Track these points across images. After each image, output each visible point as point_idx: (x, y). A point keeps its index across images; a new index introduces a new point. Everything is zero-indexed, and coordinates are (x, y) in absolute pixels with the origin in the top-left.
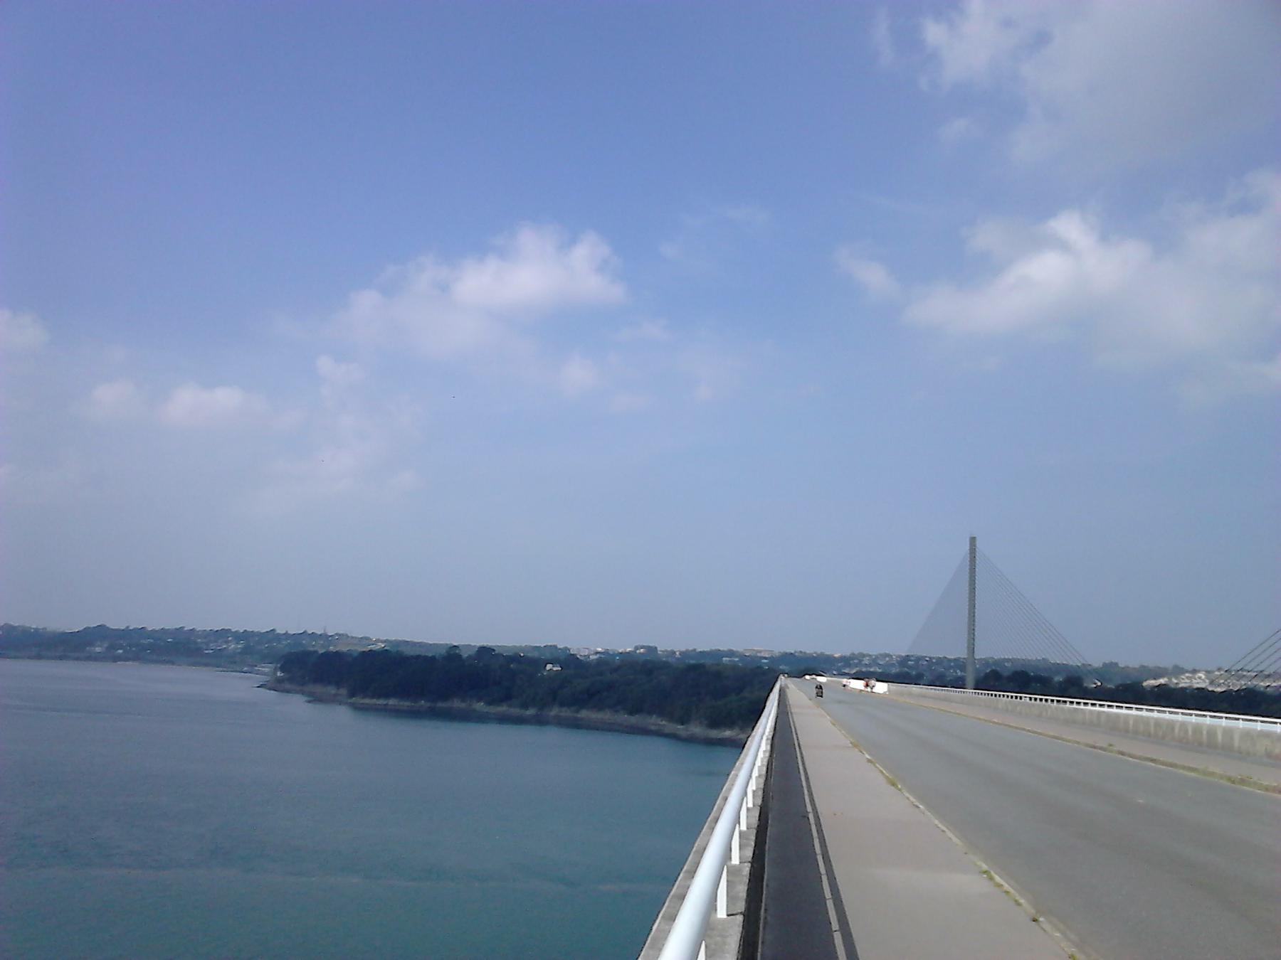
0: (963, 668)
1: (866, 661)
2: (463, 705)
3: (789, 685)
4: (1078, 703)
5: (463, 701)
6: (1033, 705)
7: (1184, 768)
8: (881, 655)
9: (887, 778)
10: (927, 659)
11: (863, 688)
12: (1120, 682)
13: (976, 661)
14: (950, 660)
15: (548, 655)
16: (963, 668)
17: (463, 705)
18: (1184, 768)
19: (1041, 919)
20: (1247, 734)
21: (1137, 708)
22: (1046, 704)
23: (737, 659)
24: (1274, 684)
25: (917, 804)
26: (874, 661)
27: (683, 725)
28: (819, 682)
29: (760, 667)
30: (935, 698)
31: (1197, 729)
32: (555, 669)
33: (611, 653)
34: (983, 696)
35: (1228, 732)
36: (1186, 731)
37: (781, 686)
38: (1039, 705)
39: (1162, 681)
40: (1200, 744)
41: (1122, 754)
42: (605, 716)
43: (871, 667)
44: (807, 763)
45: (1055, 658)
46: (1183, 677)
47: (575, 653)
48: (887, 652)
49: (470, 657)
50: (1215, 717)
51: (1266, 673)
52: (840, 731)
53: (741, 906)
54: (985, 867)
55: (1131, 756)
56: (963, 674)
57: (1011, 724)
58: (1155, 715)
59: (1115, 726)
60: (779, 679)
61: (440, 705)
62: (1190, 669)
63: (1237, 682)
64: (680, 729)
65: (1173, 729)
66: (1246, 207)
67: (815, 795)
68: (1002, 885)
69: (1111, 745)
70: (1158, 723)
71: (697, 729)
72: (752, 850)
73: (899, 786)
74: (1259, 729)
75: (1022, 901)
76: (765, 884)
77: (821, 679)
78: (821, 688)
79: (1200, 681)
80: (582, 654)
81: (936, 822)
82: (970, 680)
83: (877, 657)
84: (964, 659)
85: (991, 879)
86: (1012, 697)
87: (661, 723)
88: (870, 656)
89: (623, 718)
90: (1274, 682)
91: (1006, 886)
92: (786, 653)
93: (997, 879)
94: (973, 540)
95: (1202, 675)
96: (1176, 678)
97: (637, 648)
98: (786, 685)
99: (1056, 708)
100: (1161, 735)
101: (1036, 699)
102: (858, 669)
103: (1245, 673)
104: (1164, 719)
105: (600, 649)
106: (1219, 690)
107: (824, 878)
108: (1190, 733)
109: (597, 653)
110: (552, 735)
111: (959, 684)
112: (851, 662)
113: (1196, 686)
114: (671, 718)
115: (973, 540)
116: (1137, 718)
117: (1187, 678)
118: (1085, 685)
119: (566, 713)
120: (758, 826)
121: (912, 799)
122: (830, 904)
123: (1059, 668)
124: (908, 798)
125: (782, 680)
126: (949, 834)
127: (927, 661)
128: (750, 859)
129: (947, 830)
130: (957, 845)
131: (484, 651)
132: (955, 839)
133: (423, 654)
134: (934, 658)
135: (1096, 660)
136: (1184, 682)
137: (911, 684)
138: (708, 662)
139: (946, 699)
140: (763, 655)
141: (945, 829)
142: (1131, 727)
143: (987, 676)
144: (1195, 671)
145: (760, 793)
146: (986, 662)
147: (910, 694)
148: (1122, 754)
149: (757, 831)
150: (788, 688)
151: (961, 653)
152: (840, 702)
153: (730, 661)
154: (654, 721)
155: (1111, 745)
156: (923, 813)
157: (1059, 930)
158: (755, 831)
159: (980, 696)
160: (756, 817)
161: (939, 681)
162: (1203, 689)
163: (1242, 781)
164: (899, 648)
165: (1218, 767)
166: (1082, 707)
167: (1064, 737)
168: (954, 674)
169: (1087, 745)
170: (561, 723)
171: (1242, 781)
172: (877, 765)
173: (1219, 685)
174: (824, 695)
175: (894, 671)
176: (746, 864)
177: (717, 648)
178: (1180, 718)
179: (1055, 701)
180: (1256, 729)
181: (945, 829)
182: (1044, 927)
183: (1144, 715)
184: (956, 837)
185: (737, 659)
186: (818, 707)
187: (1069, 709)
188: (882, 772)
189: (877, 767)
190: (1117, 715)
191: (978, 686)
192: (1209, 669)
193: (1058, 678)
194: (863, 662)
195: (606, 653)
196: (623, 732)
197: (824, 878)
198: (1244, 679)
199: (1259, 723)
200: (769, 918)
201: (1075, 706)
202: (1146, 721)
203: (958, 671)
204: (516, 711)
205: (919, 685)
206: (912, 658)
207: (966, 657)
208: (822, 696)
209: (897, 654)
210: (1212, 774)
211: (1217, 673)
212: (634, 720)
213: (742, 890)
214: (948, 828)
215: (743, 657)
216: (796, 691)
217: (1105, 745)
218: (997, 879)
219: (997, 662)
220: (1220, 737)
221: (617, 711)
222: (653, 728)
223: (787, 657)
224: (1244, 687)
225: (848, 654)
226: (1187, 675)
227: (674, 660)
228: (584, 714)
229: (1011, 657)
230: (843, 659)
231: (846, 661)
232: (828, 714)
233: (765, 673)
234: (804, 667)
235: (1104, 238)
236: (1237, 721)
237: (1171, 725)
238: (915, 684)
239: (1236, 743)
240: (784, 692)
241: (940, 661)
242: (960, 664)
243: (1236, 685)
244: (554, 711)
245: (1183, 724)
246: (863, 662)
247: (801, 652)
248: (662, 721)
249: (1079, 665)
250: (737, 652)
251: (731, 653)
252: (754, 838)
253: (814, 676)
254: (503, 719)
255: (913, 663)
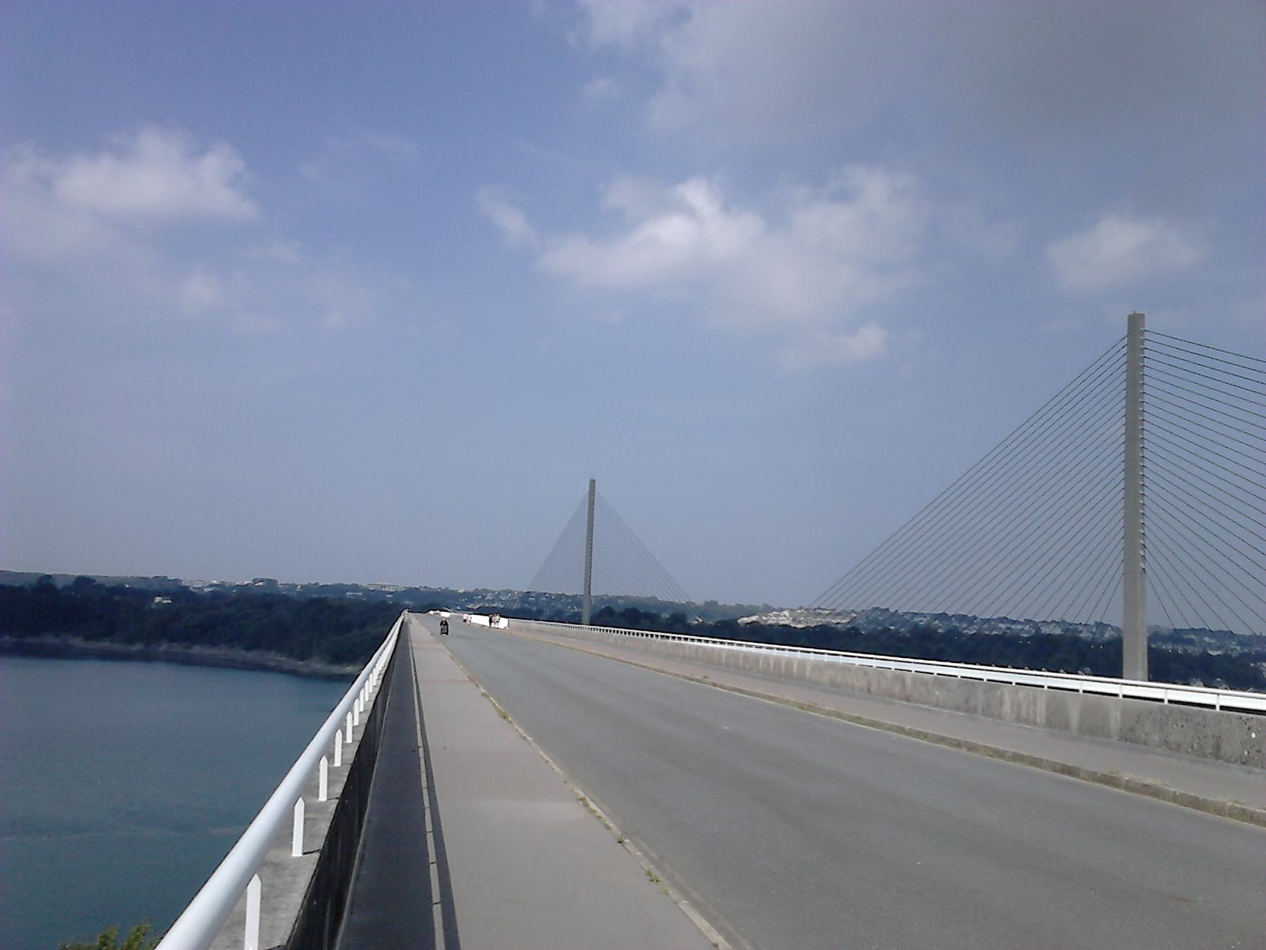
0: (579, 605)
1: (489, 597)
2: (57, 641)
3: (412, 621)
4: (680, 638)
5: (57, 636)
6: (640, 640)
7: (765, 697)
8: (504, 591)
9: (499, 711)
10: (547, 595)
11: (488, 624)
12: (719, 619)
13: (592, 599)
14: (568, 597)
15: (156, 587)
16: (579, 605)
17: (57, 641)
18: (765, 697)
19: (626, 841)
20: (817, 666)
21: (729, 643)
22: (651, 639)
23: (361, 594)
24: (843, 621)
25: (525, 735)
26: (497, 597)
27: (303, 660)
28: (443, 617)
29: (383, 602)
30: (551, 633)
31: (778, 661)
32: (164, 602)
33: (227, 585)
34: (597, 631)
35: (802, 664)
36: (769, 664)
37: (403, 619)
38: (631, 638)
39: (754, 618)
40: (780, 676)
41: (714, 685)
42: (221, 652)
43: (493, 603)
44: (422, 695)
45: (663, 597)
46: (771, 615)
47: (188, 584)
48: (511, 589)
49: (65, 588)
50: (804, 652)
51: (837, 611)
52: (459, 666)
53: (320, 843)
54: (582, 794)
55: (721, 687)
56: (580, 610)
57: (606, 655)
58: (744, 649)
59: (710, 660)
60: (403, 614)
61: (30, 640)
62: (777, 608)
63: (814, 620)
64: (299, 665)
65: (758, 663)
66: (845, 196)
67: (426, 728)
68: (595, 811)
69: (706, 677)
70: (746, 657)
71: (317, 665)
72: (344, 785)
73: (510, 719)
74: (826, 660)
75: (611, 825)
76: (365, 819)
77: (445, 615)
78: (446, 624)
79: (785, 619)
80: (196, 587)
81: (542, 753)
82: (586, 618)
83: (499, 593)
84: (581, 595)
85: (586, 805)
86: (625, 633)
87: (279, 658)
88: (493, 592)
89: (239, 654)
90: (843, 619)
91: (599, 812)
92: (412, 588)
93: (592, 806)
94: (593, 482)
95: (786, 613)
96: (766, 616)
97: (255, 581)
98: (409, 620)
99: (660, 643)
100: (783, 675)
101: (642, 635)
102: (481, 604)
103: (820, 611)
104: (751, 653)
105: (215, 582)
106: (800, 626)
107: (428, 812)
108: (772, 665)
109: (212, 586)
110: (160, 673)
111: (575, 620)
112: (475, 597)
113: (782, 623)
114: (291, 655)
115: (593, 482)
116: (730, 653)
117: (775, 616)
118: (689, 621)
119: (177, 648)
120: (354, 762)
121: (520, 730)
122: (430, 837)
123: (667, 606)
124: (517, 731)
125: (406, 615)
126: (554, 766)
127: (547, 597)
128: (339, 796)
129: (551, 761)
130: (559, 774)
131: (83, 582)
132: (558, 770)
133: (8, 584)
134: (553, 595)
135: (699, 600)
136: (771, 619)
137: (531, 619)
138: (330, 596)
139: (561, 634)
140: (387, 589)
141: (548, 759)
142: (723, 660)
143: (602, 612)
144: (781, 610)
145: (363, 729)
146: (601, 599)
147: (529, 630)
148: (714, 685)
149: (351, 768)
150: (411, 623)
151: (579, 591)
152: (461, 637)
153: (354, 595)
154: (274, 657)
155: (706, 677)
156: (530, 745)
157: (641, 850)
158: (349, 767)
159: (596, 631)
160: (353, 752)
161: (558, 617)
162: (786, 625)
163: (810, 708)
164: (520, 582)
165: (791, 695)
166: (683, 642)
167: (666, 670)
168: (572, 610)
169: (685, 678)
170: (171, 659)
171: (810, 708)
172: (492, 699)
173: (800, 622)
174: (449, 633)
175: (515, 606)
176: (334, 800)
177: (341, 582)
178: (764, 651)
179: (659, 637)
180: (824, 661)
181: (548, 759)
182: (628, 847)
183: (754, 651)
184: (560, 767)
185: (361, 594)
186: (439, 642)
187: (672, 644)
188: (494, 704)
189: (490, 700)
190: (713, 649)
191: (592, 623)
192: (792, 608)
193: (665, 615)
194: (486, 598)
195: (222, 585)
196: (240, 669)
197: (428, 812)
198: (820, 616)
199: (799, 653)
200: (367, 855)
201: (677, 641)
202: (735, 655)
203: (575, 608)
204: (119, 647)
205: (539, 620)
206: (533, 595)
207: (582, 594)
208: (447, 633)
209: (518, 590)
210: (787, 701)
211: (799, 611)
212: (251, 655)
213: (324, 827)
214: (552, 758)
215: (366, 591)
216: (419, 627)
217: (700, 678)
218: (592, 806)
219: (611, 600)
220: (783, 668)
221: (233, 646)
222: (272, 664)
223: (412, 592)
224: (819, 624)
225: (471, 589)
226: (774, 613)
227: (295, 594)
228: (197, 650)
229: (623, 595)
230: (465, 594)
231: (469, 596)
232: (448, 649)
233: (389, 608)
234: (428, 602)
235: (725, 208)
236: (771, 650)
237: (756, 658)
238: (535, 620)
239: (808, 674)
240: (407, 626)
241: (560, 597)
242: (576, 601)
243: (814, 622)
244: (164, 647)
245: (767, 657)
246: (486, 598)
247: (426, 587)
248: (281, 656)
249: (684, 603)
250: (361, 586)
251: (355, 588)
252: (347, 774)
253: (438, 612)
254: (105, 656)
255: (533, 599)
